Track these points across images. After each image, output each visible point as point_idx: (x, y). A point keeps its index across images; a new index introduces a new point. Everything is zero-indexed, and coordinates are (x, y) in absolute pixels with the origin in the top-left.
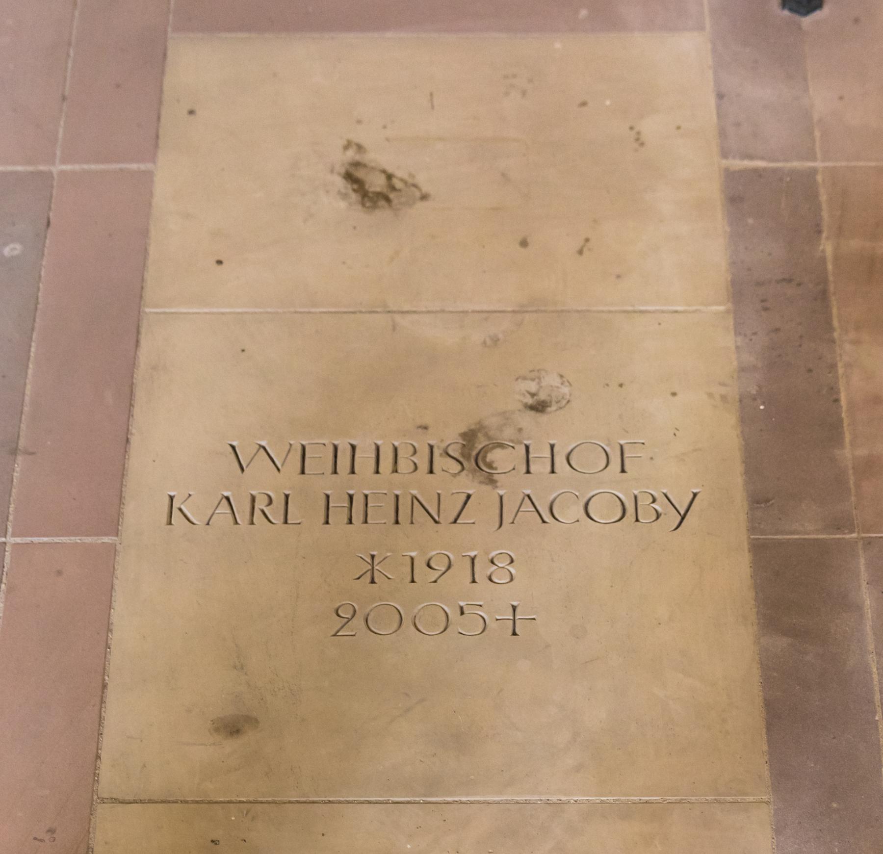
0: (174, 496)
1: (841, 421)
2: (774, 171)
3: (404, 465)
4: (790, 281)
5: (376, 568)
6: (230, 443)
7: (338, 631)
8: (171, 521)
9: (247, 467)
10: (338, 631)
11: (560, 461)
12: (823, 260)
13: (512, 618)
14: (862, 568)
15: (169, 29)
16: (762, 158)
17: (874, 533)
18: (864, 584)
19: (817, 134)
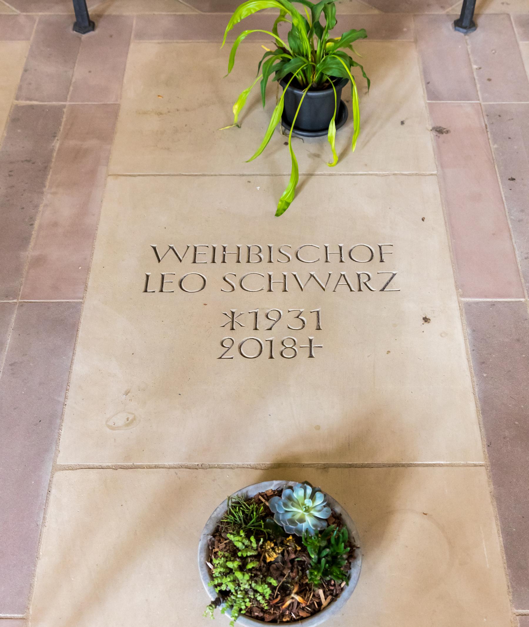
0: (331, 274)
1: (30, 235)
2: (41, 106)
3: (254, 259)
4: (28, 161)
5: (235, 320)
6: (269, 245)
7: (223, 355)
8: (285, 288)
9: (162, 259)
10: (223, 355)
11: (345, 257)
12: (52, 151)
13: (309, 346)
14: (13, 320)
15: (132, 36)
16: (36, 100)
17: (27, 300)
18: (10, 330)
19: (71, 88)
